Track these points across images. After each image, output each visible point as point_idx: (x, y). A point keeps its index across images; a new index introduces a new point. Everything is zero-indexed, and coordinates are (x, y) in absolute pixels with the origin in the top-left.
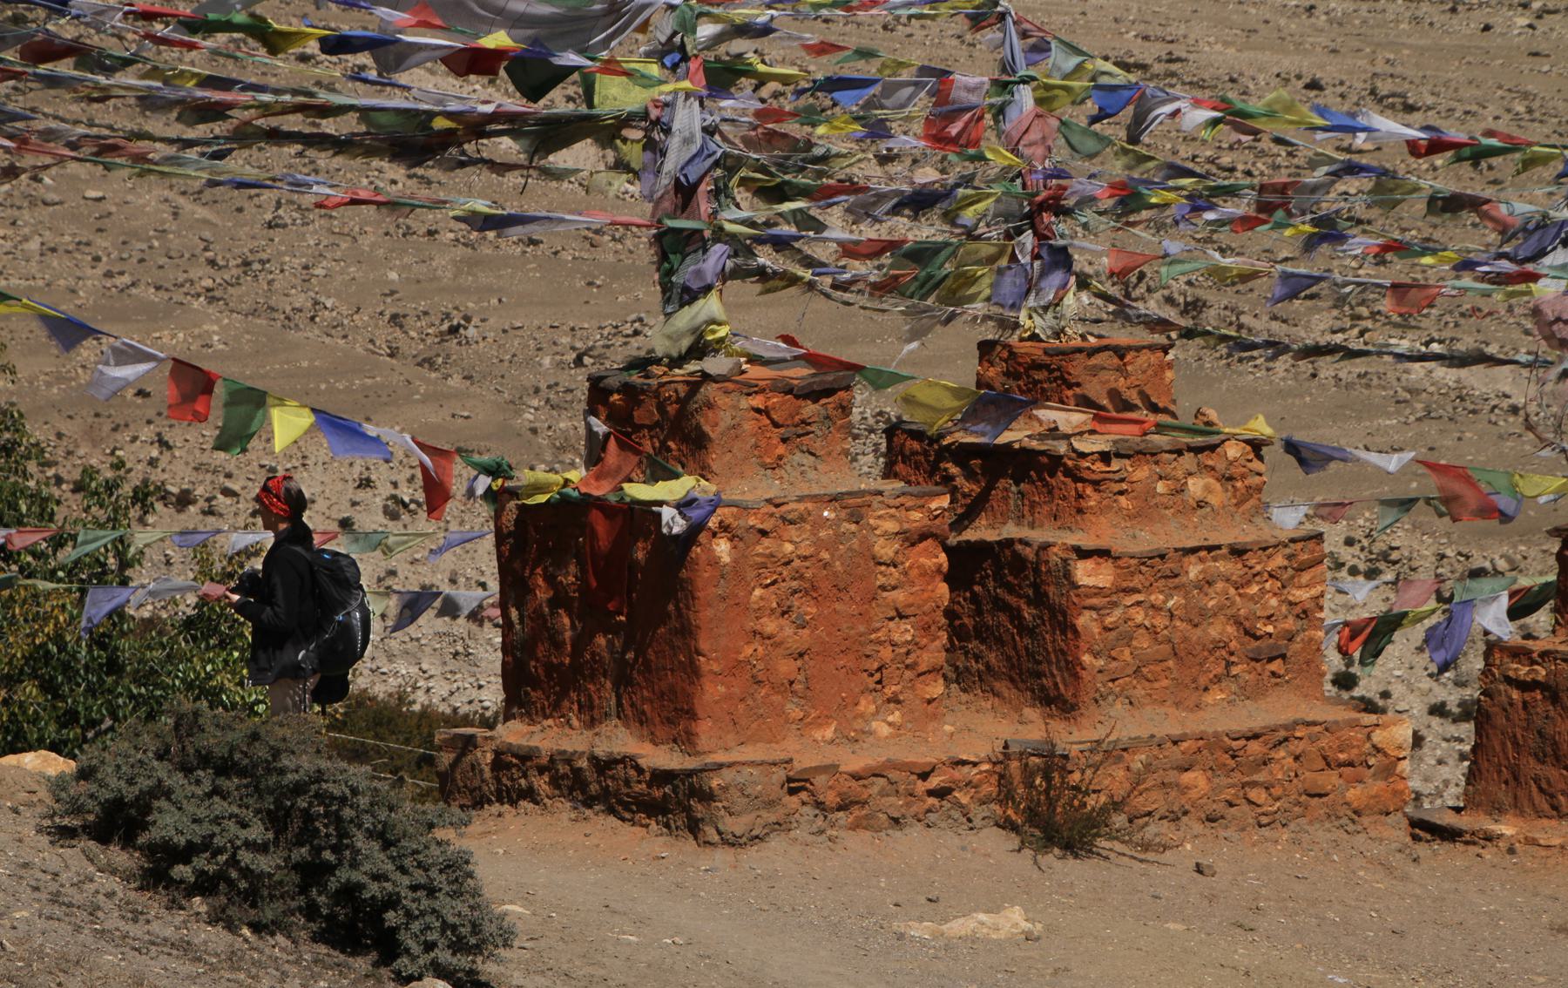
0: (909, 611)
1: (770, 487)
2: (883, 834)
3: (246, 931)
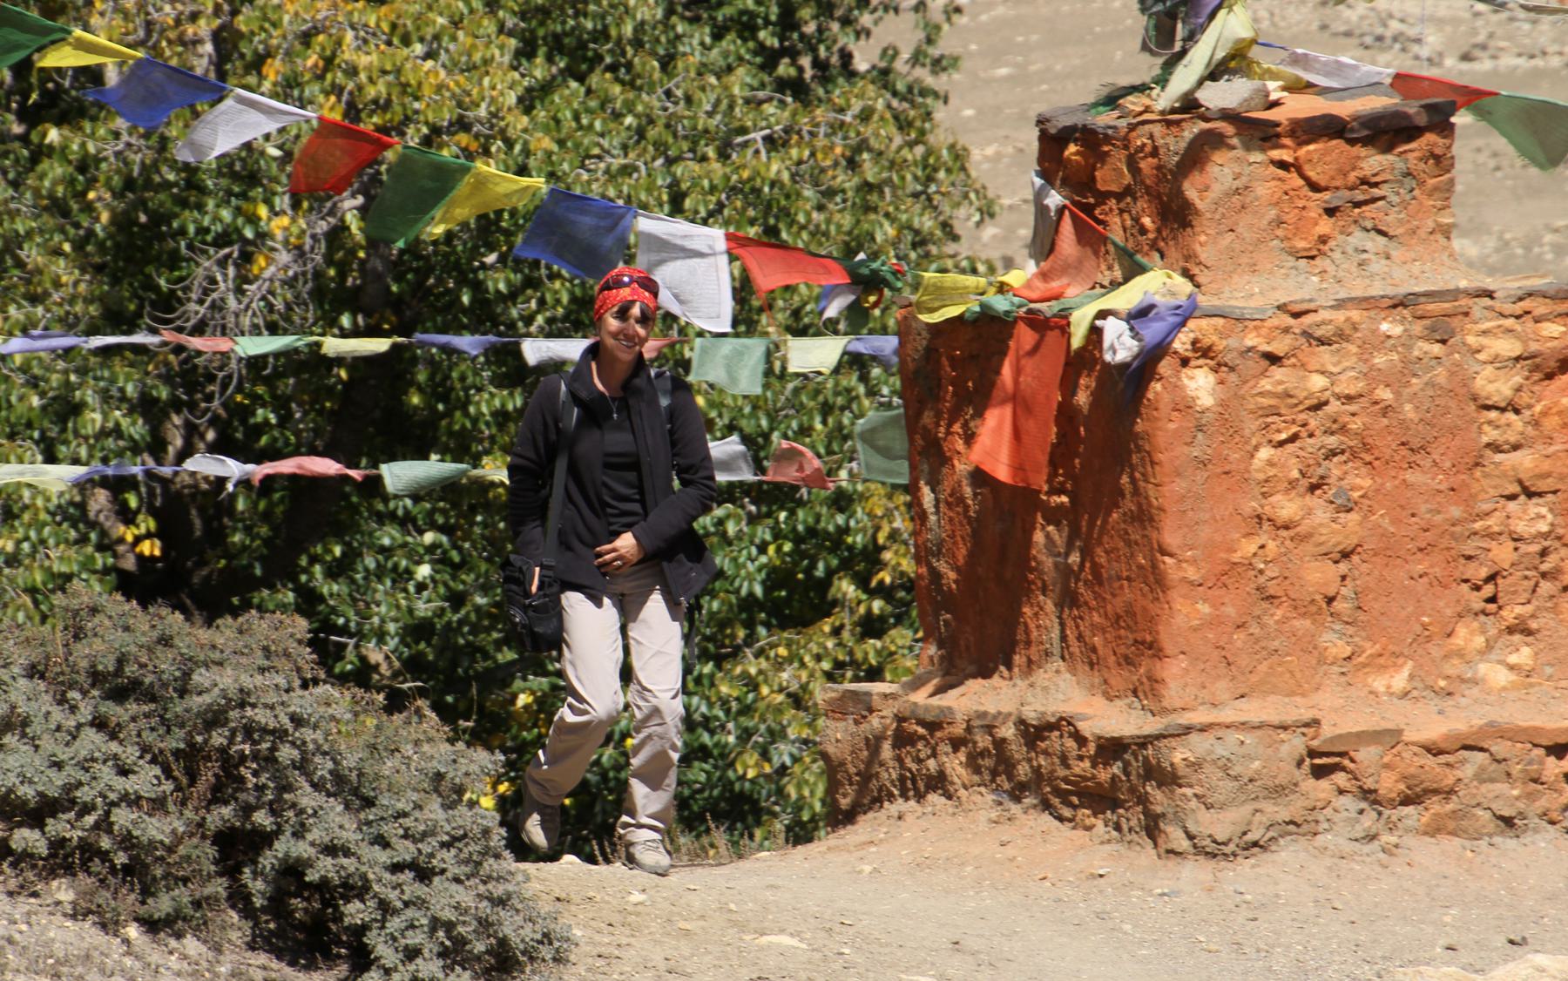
0: (1542, 486)
1: (1301, 285)
2: (1483, 843)
3: (133, 931)
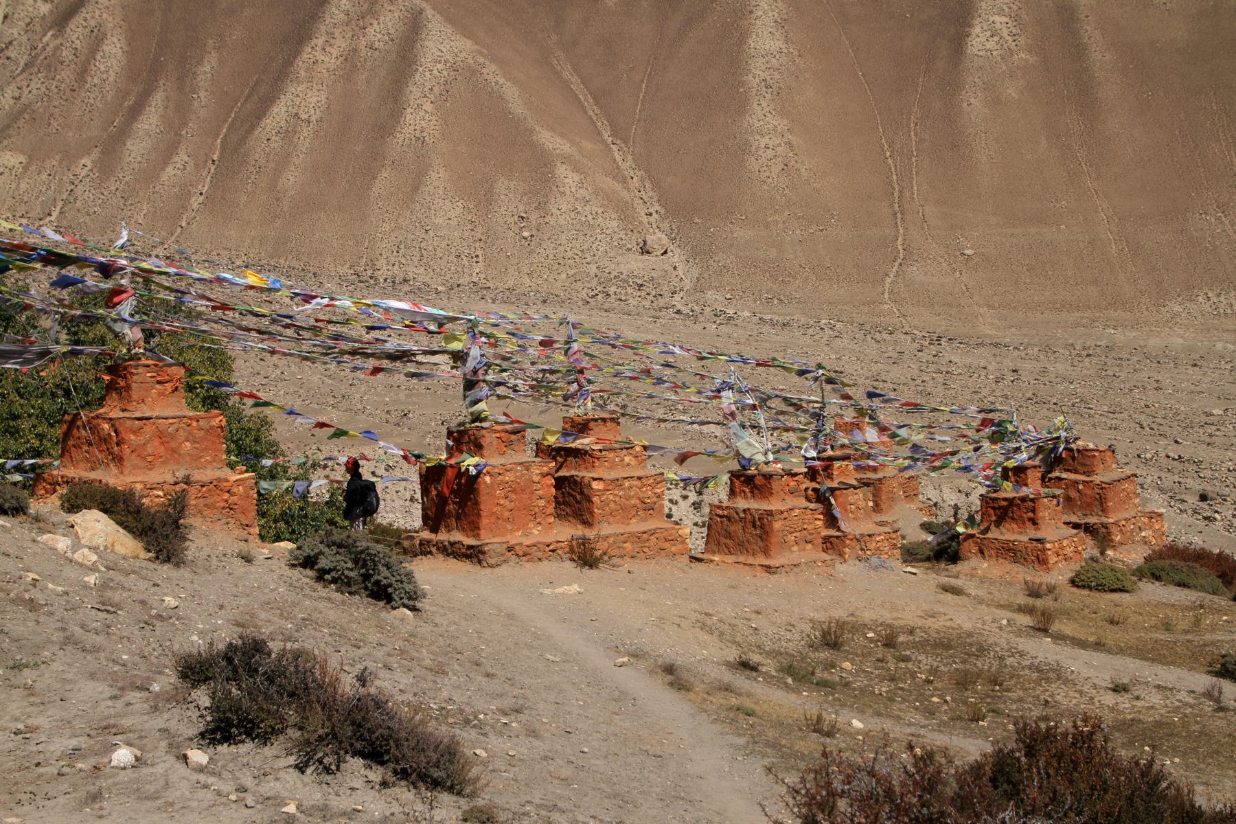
1: (502, 460)
